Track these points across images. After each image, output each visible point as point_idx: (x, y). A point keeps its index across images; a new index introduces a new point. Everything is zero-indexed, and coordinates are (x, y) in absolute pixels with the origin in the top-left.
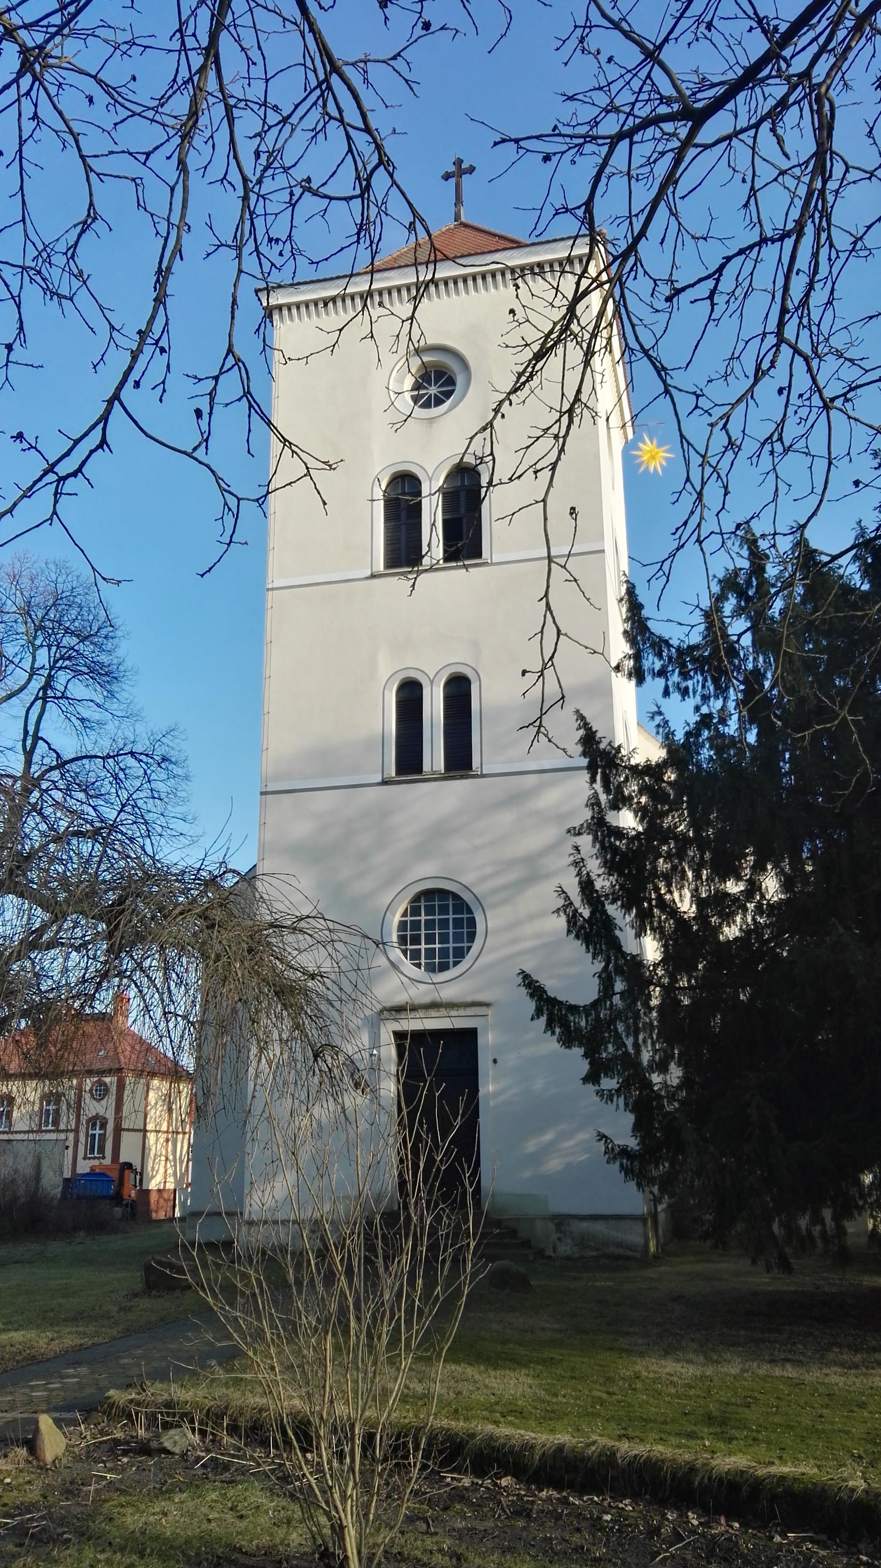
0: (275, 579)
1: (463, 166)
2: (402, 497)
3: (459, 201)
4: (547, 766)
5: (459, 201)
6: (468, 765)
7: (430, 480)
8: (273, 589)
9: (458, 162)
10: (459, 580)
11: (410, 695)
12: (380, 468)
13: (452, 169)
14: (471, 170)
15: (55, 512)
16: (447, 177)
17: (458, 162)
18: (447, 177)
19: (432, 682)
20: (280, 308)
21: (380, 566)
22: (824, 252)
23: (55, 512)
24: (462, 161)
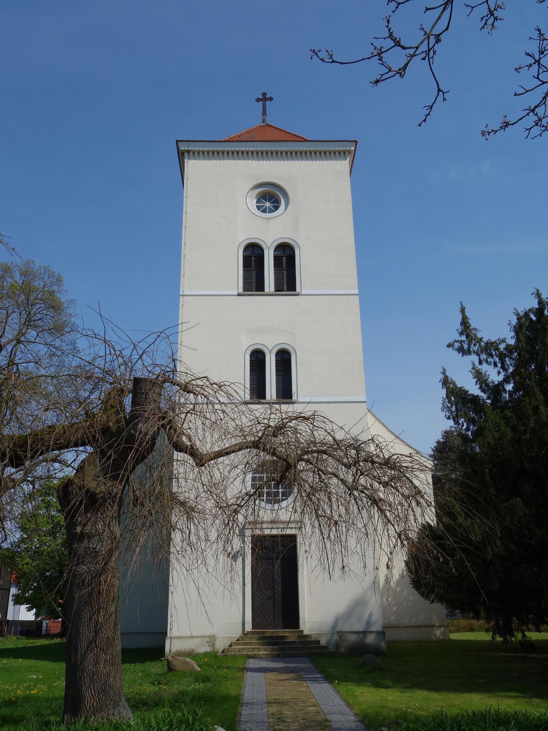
0: (186, 288)
1: (267, 97)
2: (253, 255)
3: (264, 113)
4: (331, 400)
5: (264, 113)
6: (290, 397)
7: (269, 249)
8: (183, 296)
9: (264, 94)
10: (285, 301)
11: (257, 359)
12: (243, 238)
13: (261, 97)
14: (271, 99)
15: (530, 129)
16: (258, 100)
17: (264, 94)
18: (258, 100)
19: (270, 352)
20: (189, 152)
21: (241, 290)
22: (127, 486)
23: (530, 129)
24: (266, 94)
